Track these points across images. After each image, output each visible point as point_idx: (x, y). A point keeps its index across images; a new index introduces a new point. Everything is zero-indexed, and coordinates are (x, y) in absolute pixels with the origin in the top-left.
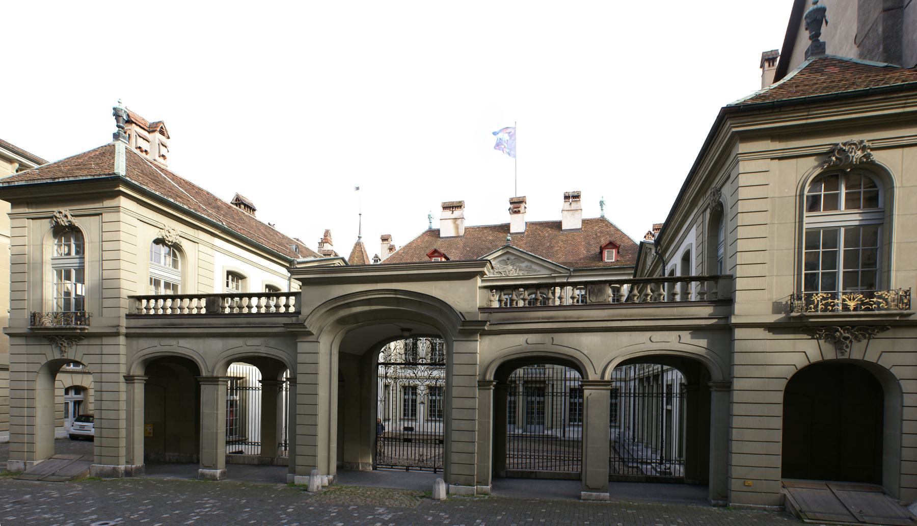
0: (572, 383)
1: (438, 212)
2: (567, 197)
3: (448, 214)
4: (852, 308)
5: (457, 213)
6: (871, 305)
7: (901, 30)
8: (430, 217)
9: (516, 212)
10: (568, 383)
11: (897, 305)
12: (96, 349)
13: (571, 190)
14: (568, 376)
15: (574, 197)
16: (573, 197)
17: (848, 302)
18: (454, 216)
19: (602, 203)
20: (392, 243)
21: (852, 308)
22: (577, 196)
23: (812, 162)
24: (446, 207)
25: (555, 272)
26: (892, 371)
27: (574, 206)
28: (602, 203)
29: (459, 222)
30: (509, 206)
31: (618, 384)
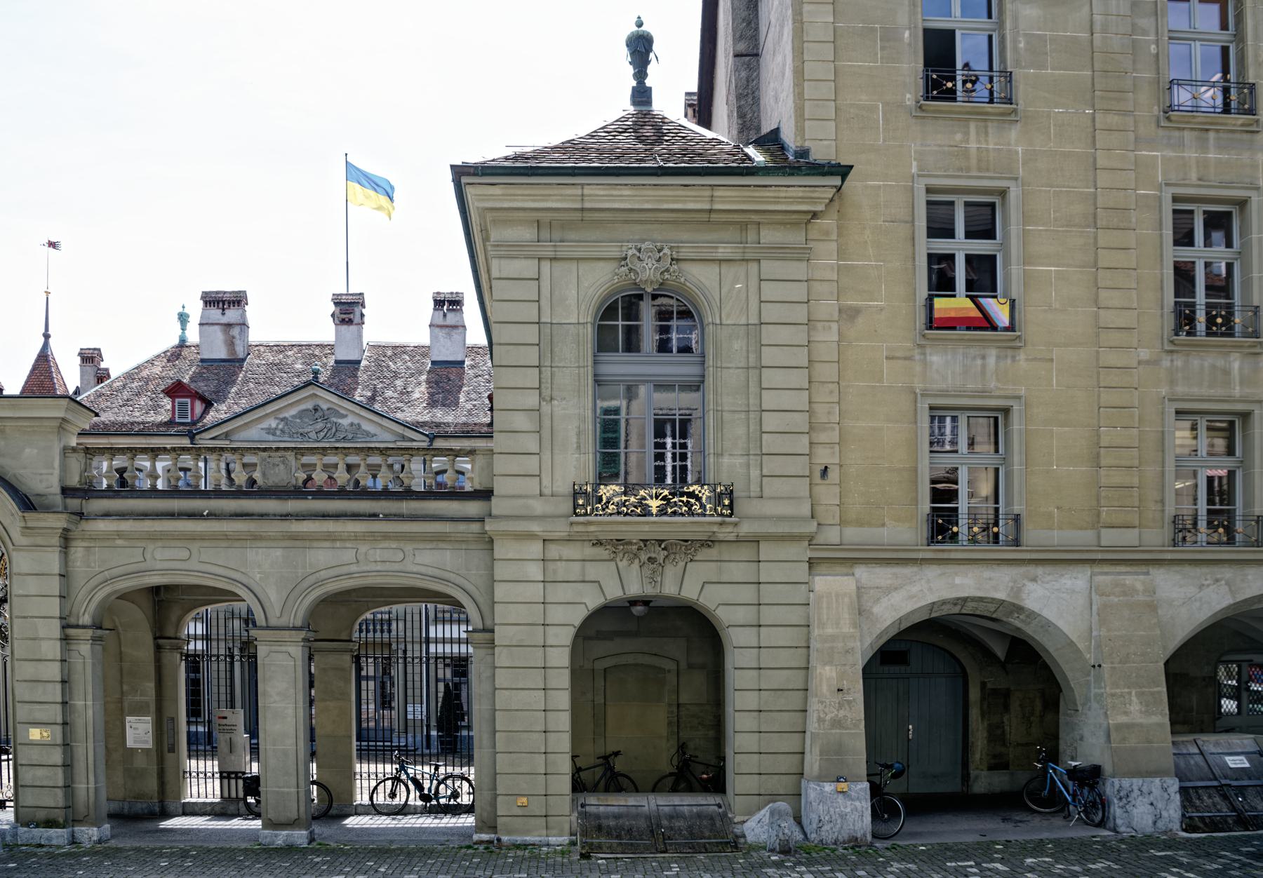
0: (440, 647)
1: (196, 309)
2: (439, 303)
3: (215, 314)
4: (654, 511)
5: (232, 315)
6: (680, 507)
7: (758, 88)
9: (343, 322)
10: (432, 648)
11: (716, 510)
12: (737, 571)
13: (53, 240)
14: (432, 635)
15: (452, 303)
16: (224, 303)
17: (649, 502)
18: (224, 320)
20: (103, 365)
21: (654, 511)
22: (237, 300)
23: (611, 266)
24: (212, 300)
25: (404, 438)
26: (934, 615)
27: (451, 319)
29: (235, 331)
30: (332, 308)
31: (463, 648)
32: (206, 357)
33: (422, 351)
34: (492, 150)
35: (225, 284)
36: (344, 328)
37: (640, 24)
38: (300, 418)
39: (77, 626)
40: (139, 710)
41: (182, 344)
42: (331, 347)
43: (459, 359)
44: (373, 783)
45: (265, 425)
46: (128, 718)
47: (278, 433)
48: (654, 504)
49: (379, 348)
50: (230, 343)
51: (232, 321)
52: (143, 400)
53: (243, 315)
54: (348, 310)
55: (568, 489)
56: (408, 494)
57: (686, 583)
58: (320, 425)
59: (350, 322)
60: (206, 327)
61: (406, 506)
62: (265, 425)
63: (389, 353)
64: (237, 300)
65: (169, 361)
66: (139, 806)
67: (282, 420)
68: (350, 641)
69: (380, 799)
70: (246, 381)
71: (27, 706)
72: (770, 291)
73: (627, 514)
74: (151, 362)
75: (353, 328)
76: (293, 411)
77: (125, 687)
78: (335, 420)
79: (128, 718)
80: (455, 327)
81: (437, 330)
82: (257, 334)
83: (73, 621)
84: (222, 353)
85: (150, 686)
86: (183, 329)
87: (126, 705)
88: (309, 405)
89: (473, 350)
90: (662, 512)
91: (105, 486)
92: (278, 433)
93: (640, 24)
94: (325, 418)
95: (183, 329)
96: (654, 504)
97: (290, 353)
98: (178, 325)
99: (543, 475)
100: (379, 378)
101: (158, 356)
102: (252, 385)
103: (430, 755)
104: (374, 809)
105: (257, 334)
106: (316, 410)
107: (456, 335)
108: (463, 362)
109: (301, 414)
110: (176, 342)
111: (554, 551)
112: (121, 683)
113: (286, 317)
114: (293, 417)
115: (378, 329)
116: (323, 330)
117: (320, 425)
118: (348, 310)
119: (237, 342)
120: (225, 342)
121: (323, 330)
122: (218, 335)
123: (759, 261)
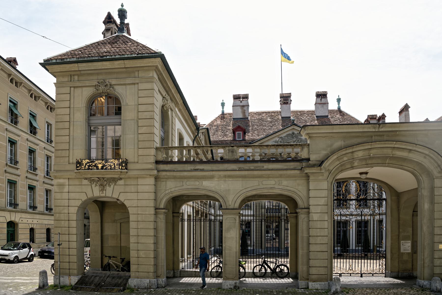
3: (238, 102)
4: (100, 168)
8: (223, 105)
9: (285, 103)
16: (322, 96)
18: (242, 104)
19: (339, 100)
21: (100, 168)
22: (246, 97)
24: (236, 97)
27: (323, 100)
28: (339, 100)
29: (245, 108)
32: (235, 117)
33: (279, 113)
34: (399, 110)
35: (321, 90)
36: (285, 105)
37: (122, 6)
38: (287, 137)
39: (160, 209)
40: (406, 238)
41: (223, 113)
42: (280, 112)
43: (327, 115)
44: (255, 265)
45: (274, 140)
46: (402, 242)
47: (279, 142)
48: (100, 166)
49: (296, 112)
50: (244, 112)
51: (244, 105)
52: (220, 133)
53: (248, 103)
54: (286, 99)
55: (75, 161)
56: (172, 162)
57: (111, 193)
58: (295, 139)
59: (287, 103)
60: (235, 107)
61: (252, 166)
62: (274, 140)
63: (299, 114)
64: (246, 97)
65: (221, 119)
66: (405, 274)
67: (281, 138)
68: (179, 213)
69: (257, 270)
70: (253, 126)
71: (439, 236)
72: (141, 94)
73: (91, 169)
74: (215, 120)
75: (287, 105)
76: (285, 135)
77: (401, 230)
78: (299, 137)
79: (402, 242)
80: (325, 104)
81: (318, 105)
82: (252, 109)
83: (158, 207)
84: (241, 116)
85: (411, 229)
86: (223, 108)
87: (401, 236)
88: (290, 132)
89: (332, 112)
90: (102, 168)
91: (192, 160)
92: (279, 142)
93: (122, 6)
94: (296, 137)
95: (223, 108)
96: (100, 166)
97: (263, 115)
98: (221, 107)
99: (137, 156)
100: (300, 123)
101: (217, 118)
102: (256, 127)
103: (358, 257)
104: (254, 275)
105: (252, 109)
106: (293, 134)
107: (325, 106)
108: (328, 116)
109: (288, 136)
110: (221, 113)
111: (71, 182)
112: (399, 228)
113: (264, 102)
114: (285, 136)
115: (295, 106)
116: (276, 106)
117: (295, 139)
118: (286, 99)
119: (246, 112)
120: (242, 112)
121: (276, 106)
122: (239, 109)
123: (138, 83)
